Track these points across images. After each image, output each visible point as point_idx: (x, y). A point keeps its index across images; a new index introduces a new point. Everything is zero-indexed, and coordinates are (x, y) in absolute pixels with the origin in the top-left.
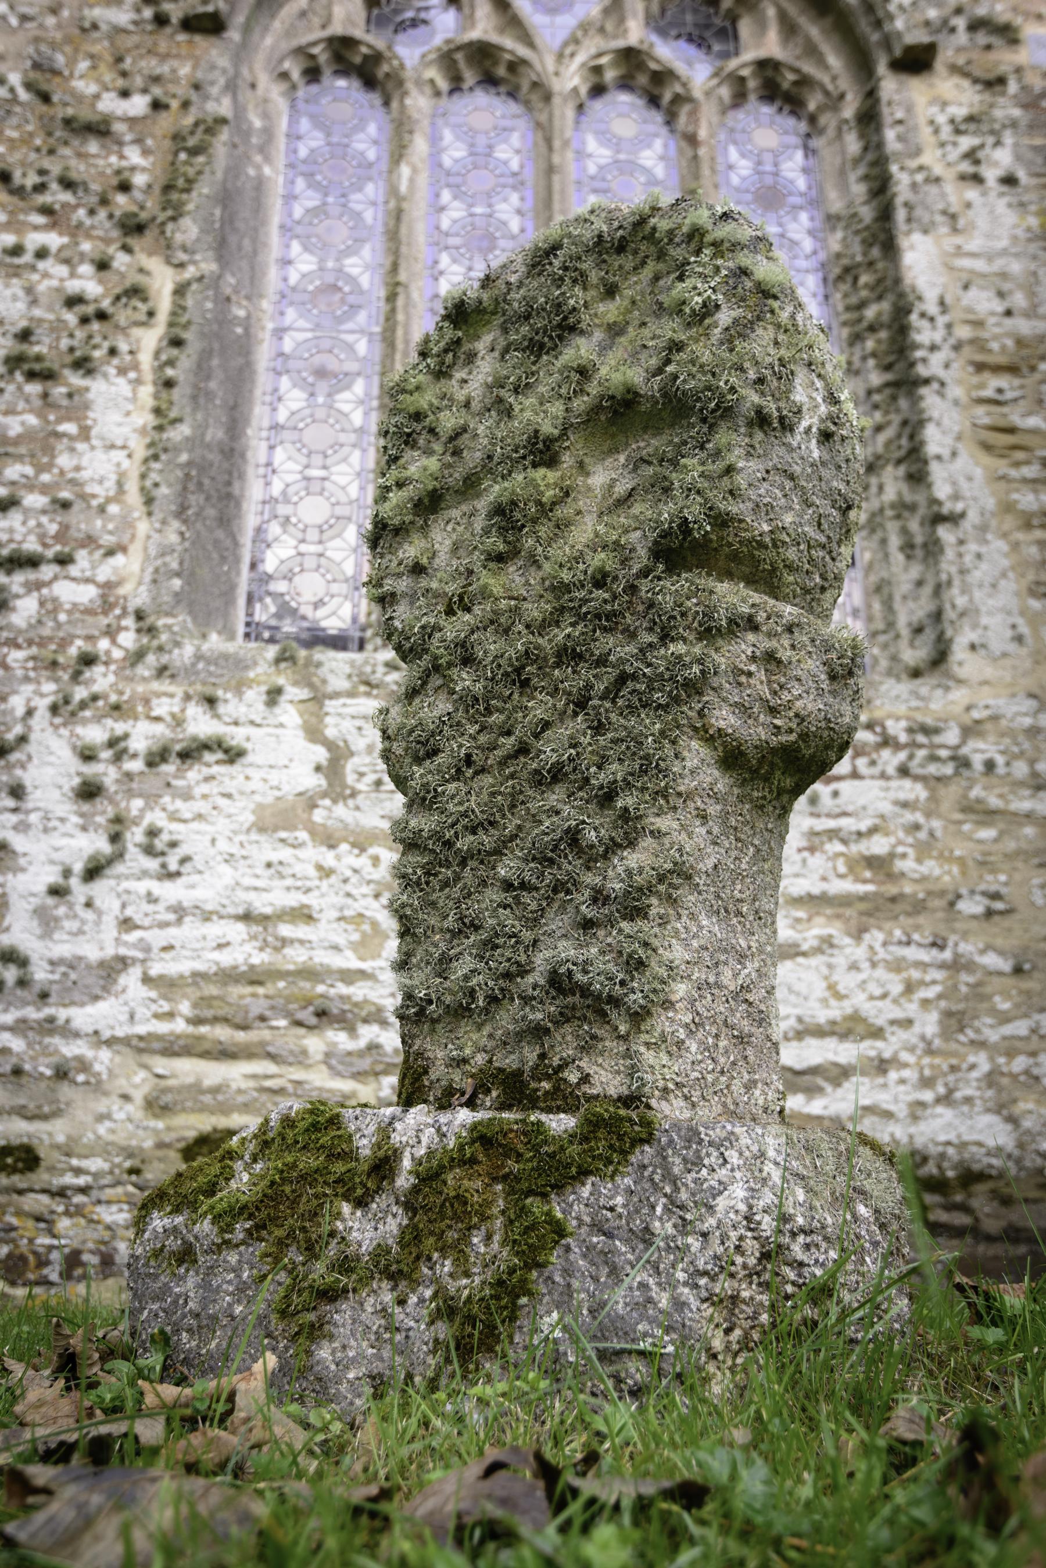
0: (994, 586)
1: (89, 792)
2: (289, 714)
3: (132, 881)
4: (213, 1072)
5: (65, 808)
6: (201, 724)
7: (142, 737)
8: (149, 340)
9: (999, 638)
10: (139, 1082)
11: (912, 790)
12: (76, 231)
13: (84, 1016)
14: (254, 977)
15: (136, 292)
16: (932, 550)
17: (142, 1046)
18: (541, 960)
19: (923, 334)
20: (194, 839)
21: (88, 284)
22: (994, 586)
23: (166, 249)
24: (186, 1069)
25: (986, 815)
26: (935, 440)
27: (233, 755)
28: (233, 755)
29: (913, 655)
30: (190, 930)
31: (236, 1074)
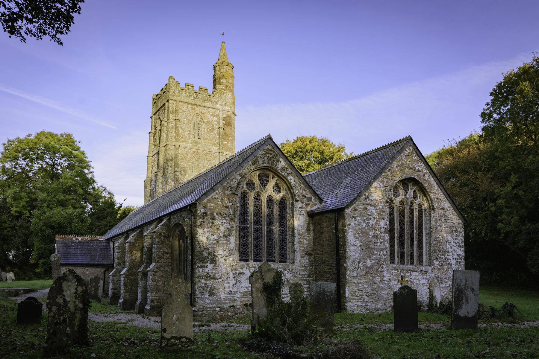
0: (223, 76)
1: (234, 277)
2: (248, 270)
3: (238, 284)
4: (245, 299)
5: (233, 279)
6: (242, 271)
7: (238, 272)
8: (234, 232)
9: (298, 262)
10: (240, 300)
11: (291, 275)
12: (227, 220)
13: (236, 295)
14: (247, 292)
15: (233, 227)
16: (294, 253)
17: (240, 298)
18: (508, 188)
19: (295, 232)
20: (242, 281)
21: (228, 226)
22: (223, 76)
23: (235, 222)
24: (243, 299)
25: (295, 277)
26: (295, 243)
27: (244, 274)
28: (244, 274)
29: (291, 262)
30: (242, 288)
31: (246, 299)
